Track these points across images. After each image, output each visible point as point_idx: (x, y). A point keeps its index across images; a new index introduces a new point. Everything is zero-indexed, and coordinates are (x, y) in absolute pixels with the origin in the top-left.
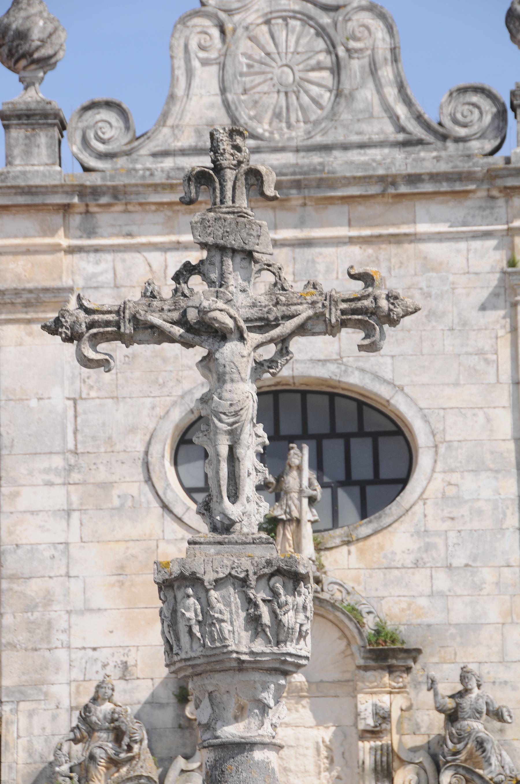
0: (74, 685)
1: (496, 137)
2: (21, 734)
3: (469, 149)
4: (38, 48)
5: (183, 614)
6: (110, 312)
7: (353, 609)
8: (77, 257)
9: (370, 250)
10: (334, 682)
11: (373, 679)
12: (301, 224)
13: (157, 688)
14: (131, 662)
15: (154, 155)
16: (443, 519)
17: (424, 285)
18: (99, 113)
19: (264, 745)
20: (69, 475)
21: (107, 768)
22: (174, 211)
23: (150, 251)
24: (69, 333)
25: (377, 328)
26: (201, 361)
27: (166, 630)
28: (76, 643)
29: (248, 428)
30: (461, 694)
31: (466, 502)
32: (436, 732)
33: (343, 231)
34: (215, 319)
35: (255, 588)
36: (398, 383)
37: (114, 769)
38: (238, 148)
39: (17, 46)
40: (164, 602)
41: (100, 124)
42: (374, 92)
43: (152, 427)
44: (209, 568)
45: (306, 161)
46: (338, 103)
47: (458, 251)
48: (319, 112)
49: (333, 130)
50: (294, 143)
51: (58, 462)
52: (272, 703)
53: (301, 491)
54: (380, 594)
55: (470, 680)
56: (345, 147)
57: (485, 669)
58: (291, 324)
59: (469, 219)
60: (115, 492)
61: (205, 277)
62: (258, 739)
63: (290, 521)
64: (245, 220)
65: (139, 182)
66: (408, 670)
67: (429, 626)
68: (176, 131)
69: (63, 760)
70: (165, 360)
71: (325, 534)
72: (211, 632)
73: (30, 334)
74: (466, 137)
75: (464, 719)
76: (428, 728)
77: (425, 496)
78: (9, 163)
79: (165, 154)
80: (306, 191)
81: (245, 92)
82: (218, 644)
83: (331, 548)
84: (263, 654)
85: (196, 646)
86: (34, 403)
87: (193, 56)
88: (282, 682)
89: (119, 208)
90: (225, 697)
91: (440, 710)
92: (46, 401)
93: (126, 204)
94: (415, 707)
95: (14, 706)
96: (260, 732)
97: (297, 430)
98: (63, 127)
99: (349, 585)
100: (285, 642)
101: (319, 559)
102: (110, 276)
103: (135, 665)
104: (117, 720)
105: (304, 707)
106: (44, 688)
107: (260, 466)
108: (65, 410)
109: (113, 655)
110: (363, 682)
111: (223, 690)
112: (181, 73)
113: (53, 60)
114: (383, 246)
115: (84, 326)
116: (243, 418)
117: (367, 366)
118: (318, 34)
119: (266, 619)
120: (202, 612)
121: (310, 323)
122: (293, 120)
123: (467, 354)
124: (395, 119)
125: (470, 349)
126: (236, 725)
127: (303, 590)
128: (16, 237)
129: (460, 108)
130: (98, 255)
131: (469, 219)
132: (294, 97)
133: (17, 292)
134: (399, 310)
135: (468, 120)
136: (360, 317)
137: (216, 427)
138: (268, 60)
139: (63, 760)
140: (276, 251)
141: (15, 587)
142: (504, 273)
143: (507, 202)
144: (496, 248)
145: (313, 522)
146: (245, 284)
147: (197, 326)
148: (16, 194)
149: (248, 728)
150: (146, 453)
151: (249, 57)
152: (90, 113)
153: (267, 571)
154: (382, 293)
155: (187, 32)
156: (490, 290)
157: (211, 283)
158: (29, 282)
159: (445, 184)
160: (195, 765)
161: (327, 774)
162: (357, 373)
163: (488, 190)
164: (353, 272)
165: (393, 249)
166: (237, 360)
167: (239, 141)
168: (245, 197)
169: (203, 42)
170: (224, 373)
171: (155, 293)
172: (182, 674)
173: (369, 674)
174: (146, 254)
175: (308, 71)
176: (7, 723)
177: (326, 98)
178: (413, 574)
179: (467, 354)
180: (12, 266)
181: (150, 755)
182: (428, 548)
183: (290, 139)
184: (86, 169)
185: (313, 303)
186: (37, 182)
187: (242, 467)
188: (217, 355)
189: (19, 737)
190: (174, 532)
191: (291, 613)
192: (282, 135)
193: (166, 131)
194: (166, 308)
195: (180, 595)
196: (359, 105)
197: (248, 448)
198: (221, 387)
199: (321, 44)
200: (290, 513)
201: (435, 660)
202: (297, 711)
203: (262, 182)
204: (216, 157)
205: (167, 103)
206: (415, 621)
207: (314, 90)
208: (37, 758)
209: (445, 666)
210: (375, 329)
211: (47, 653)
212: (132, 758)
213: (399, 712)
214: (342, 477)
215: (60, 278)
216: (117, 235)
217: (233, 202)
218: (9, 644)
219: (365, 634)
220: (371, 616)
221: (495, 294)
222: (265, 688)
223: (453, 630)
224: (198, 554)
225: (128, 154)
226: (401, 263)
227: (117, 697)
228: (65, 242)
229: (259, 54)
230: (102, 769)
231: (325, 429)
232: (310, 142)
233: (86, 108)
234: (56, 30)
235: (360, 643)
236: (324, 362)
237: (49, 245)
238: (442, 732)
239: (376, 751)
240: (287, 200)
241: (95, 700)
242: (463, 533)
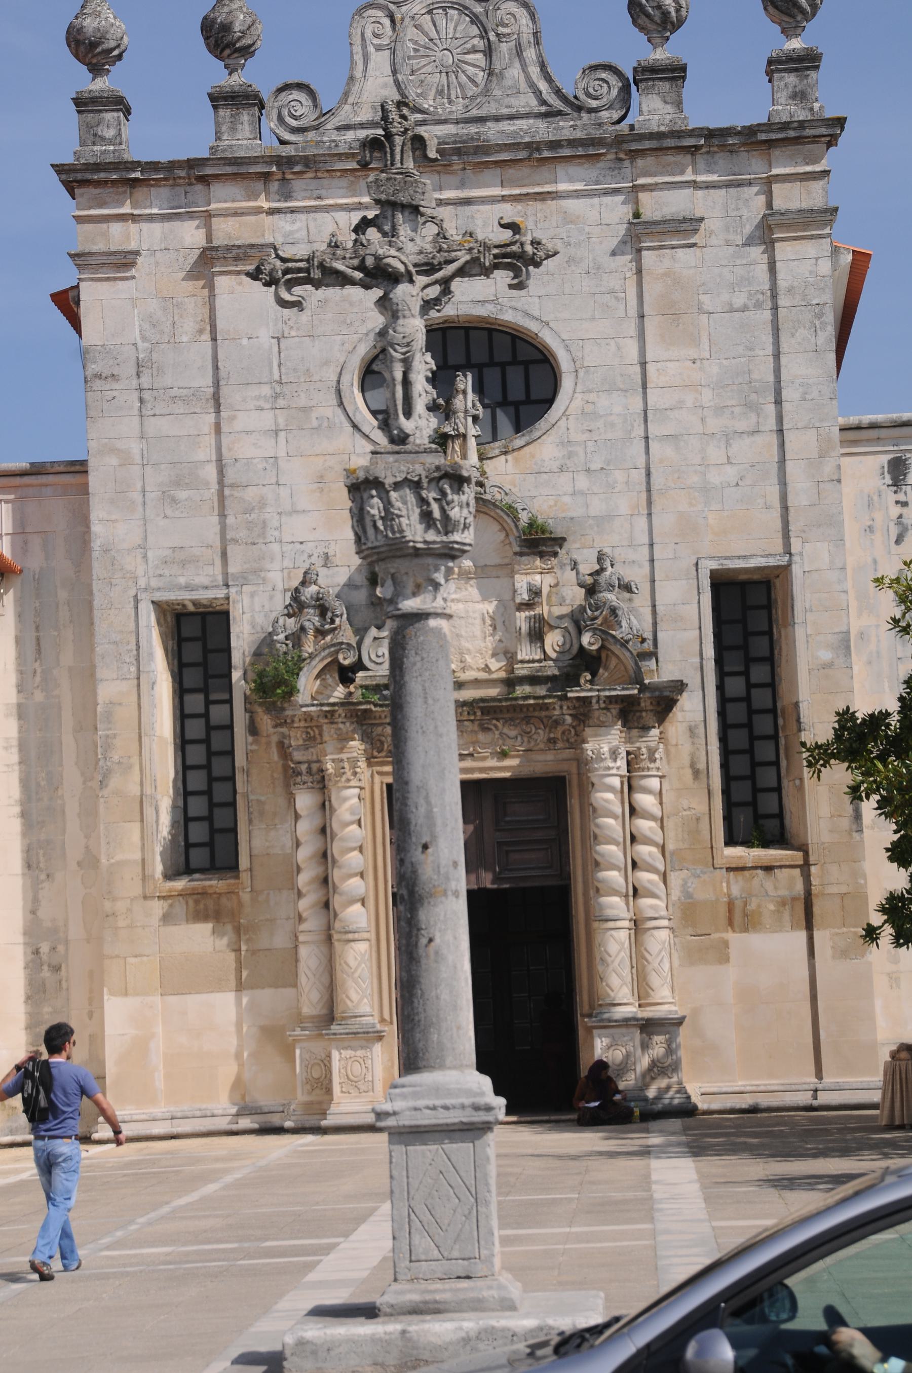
0: (286, 571)
2: (246, 610)
4: (239, 39)
5: (369, 512)
6: (301, 261)
7: (511, 507)
8: (276, 217)
9: (519, 207)
10: (495, 566)
11: (526, 562)
12: (462, 185)
13: (353, 573)
15: (338, 129)
16: (583, 432)
17: (564, 235)
18: (291, 94)
19: (437, 615)
20: (275, 402)
21: (315, 637)
24: (268, 278)
25: (524, 269)
26: (378, 301)
27: (355, 524)
28: (287, 538)
29: (418, 357)
30: (598, 573)
31: (601, 416)
32: (578, 602)
33: (497, 191)
34: (388, 265)
35: (427, 489)
37: (320, 638)
38: (404, 117)
39: (222, 37)
40: (353, 502)
41: (292, 103)
42: (521, 71)
43: (342, 360)
44: (389, 474)
47: (592, 206)
50: (454, 116)
51: (266, 390)
52: (442, 581)
53: (466, 411)
55: (605, 561)
56: (497, 119)
57: (618, 551)
58: (452, 268)
60: (314, 415)
61: (380, 230)
62: (432, 610)
63: (458, 436)
64: (411, 179)
66: (555, 554)
67: (572, 519)
68: (356, 108)
69: (280, 631)
70: (351, 304)
72: (392, 526)
73: (240, 284)
75: (601, 592)
76: (572, 600)
77: (567, 413)
78: (218, 138)
79: (347, 127)
81: (413, 73)
82: (398, 535)
83: (492, 458)
84: (434, 542)
85: (379, 537)
86: (245, 341)
87: (368, 42)
88: (451, 564)
90: (405, 578)
93: (316, 171)
94: (561, 584)
95: (239, 588)
96: (434, 604)
97: (462, 360)
98: (262, 106)
99: (507, 488)
100: (452, 532)
102: (305, 233)
103: (335, 556)
105: (472, 586)
106: (262, 574)
107: (429, 388)
108: (271, 348)
109: (316, 547)
110: (519, 565)
111: (403, 572)
112: (358, 57)
113: (252, 49)
115: (280, 273)
117: (519, 305)
118: (472, 22)
119: (437, 514)
121: (468, 266)
122: (453, 96)
123: (601, 293)
124: (538, 93)
125: (603, 289)
126: (414, 599)
128: (225, 201)
129: (592, 84)
130: (294, 215)
133: (228, 248)
134: (541, 254)
136: (509, 260)
137: (392, 356)
138: (431, 45)
139: (280, 631)
140: (441, 209)
141: (236, 494)
142: (630, 223)
143: (632, 163)
144: (623, 203)
145: (476, 437)
146: (413, 234)
147: (374, 271)
148: (224, 165)
149: (424, 602)
150: (338, 382)
151: (416, 43)
153: (436, 474)
155: (363, 22)
156: (619, 238)
157: (385, 234)
159: (580, 149)
160: (385, 633)
161: (491, 638)
162: (510, 311)
165: (539, 205)
166: (408, 299)
167: (405, 111)
168: (411, 159)
169: (376, 30)
170: (397, 311)
171: (339, 244)
173: (524, 558)
175: (465, 54)
176: (234, 602)
177: (481, 76)
178: (559, 476)
179: (601, 293)
181: (349, 626)
182: (570, 455)
184: (282, 142)
185: (471, 249)
186: (242, 154)
187: (414, 389)
188: (391, 296)
189: (243, 613)
191: (457, 509)
193: (347, 107)
194: (348, 256)
195: (365, 496)
196: (508, 82)
197: (419, 373)
198: (395, 323)
199: (475, 30)
200: (457, 430)
201: (577, 546)
202: (466, 589)
203: (425, 146)
205: (348, 84)
207: (471, 70)
208: (259, 629)
209: (585, 551)
210: (522, 270)
211: (264, 546)
212: (335, 629)
213: (549, 588)
214: (499, 398)
215: (263, 235)
216: (309, 198)
217: (402, 164)
218: (233, 539)
219: (520, 527)
221: (623, 242)
222: (437, 570)
223: (591, 522)
224: (380, 462)
225: (316, 128)
227: (321, 581)
228: (266, 205)
229: (423, 40)
231: (485, 359)
233: (280, 90)
234: (254, 22)
235: (517, 534)
237: (253, 208)
238: (583, 603)
239: (530, 618)
241: (303, 583)
242: (599, 442)
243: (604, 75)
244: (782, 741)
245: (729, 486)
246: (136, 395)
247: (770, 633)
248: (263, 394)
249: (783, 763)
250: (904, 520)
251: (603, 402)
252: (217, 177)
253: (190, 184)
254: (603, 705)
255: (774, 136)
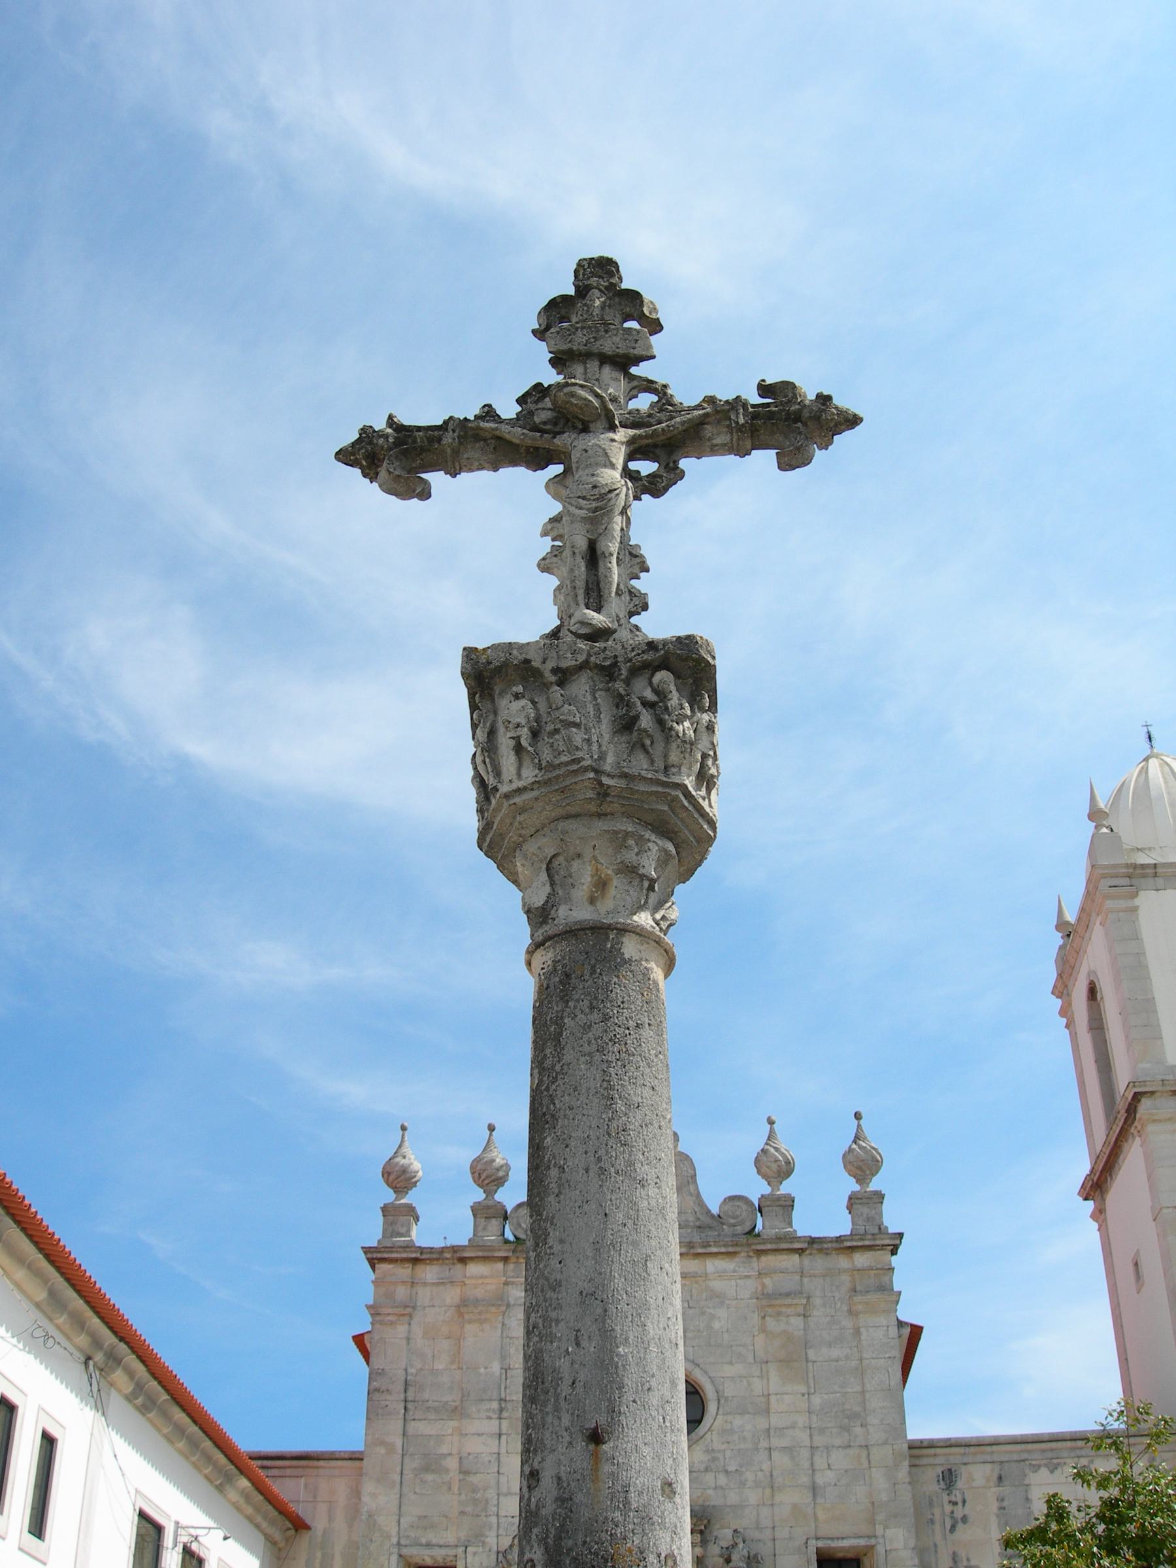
86: (482, 1370)
182: (714, 1459)
243: (738, 1203)
245: (830, 1485)
246: (402, 1405)
248: (492, 1407)
250: (955, 1515)
251: (738, 1421)
252: (472, 1259)
253: (453, 1264)
255: (855, 1244)
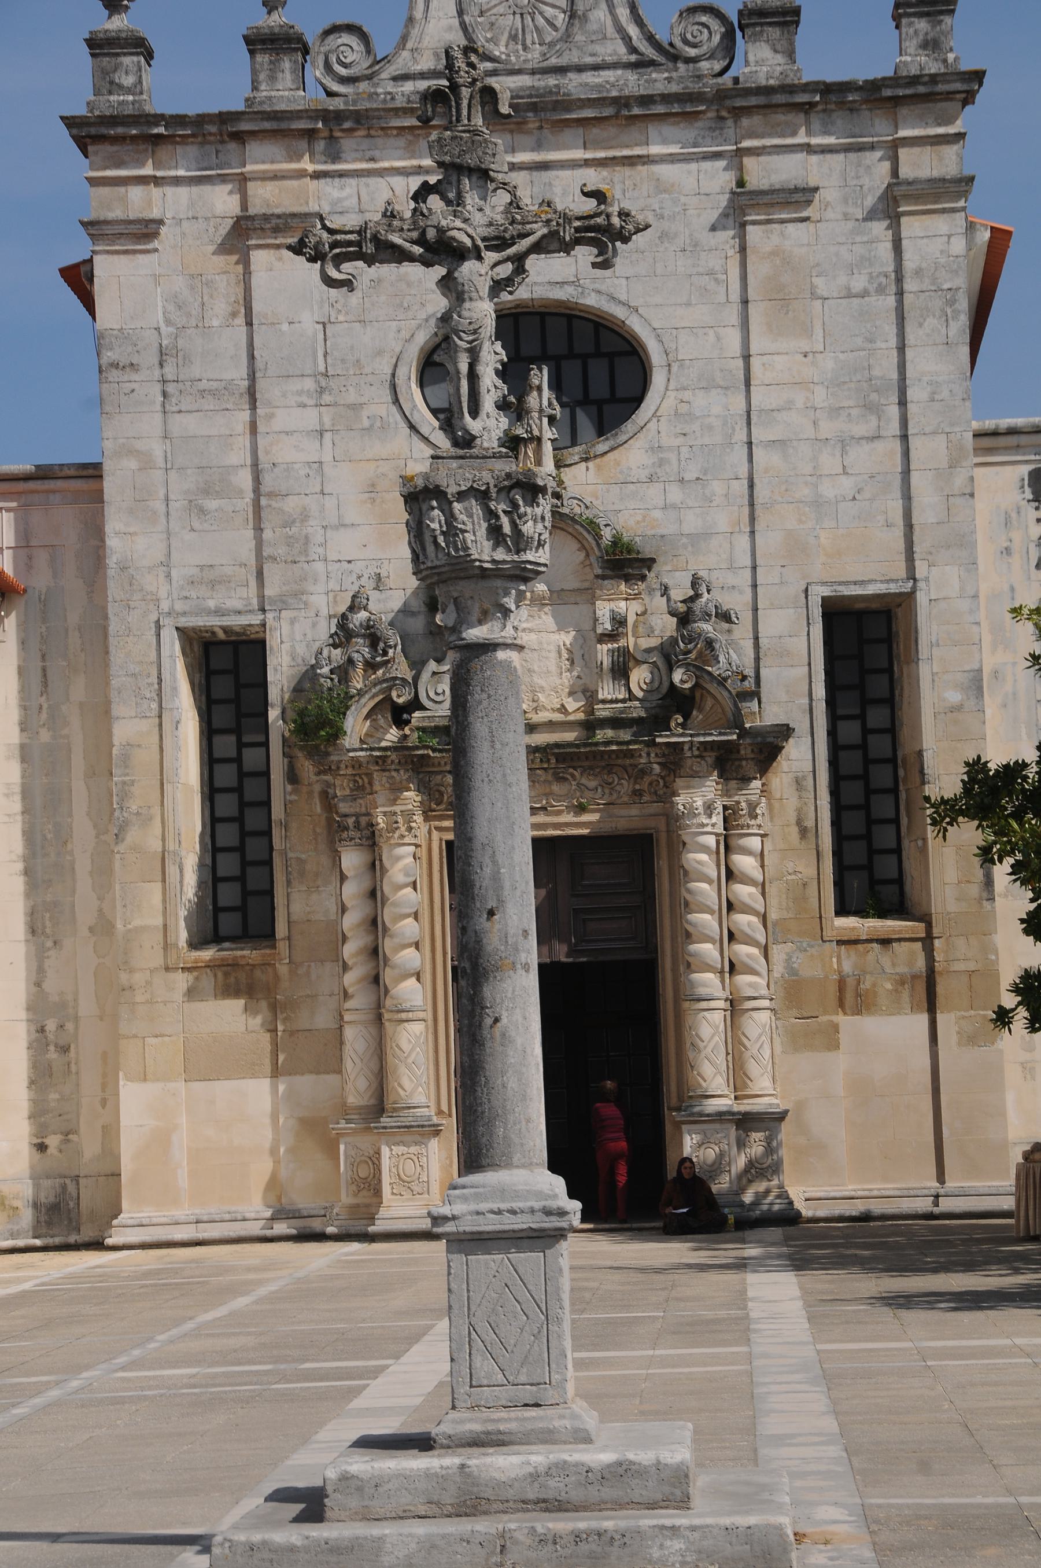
0: (331, 595)
1: (724, 58)
3: (699, 69)
7: (592, 522)
8: (322, 181)
9: (605, 173)
10: (573, 590)
11: (610, 587)
12: (538, 147)
14: (384, 574)
15: (395, 79)
16: (676, 436)
17: (656, 207)
18: (340, 37)
19: (506, 646)
20: (320, 397)
22: (415, 136)
23: (394, 175)
24: (312, 253)
26: (440, 281)
27: (413, 540)
28: (332, 556)
29: (486, 346)
31: (697, 418)
32: (669, 634)
33: (579, 154)
34: (453, 238)
36: (632, 304)
37: (370, 671)
38: (472, 65)
41: (342, 48)
42: (607, 13)
43: (398, 350)
45: (542, 83)
46: (573, 25)
47: (689, 172)
48: (554, 33)
49: (568, 52)
50: (529, 66)
52: (513, 607)
53: (541, 411)
54: (616, 507)
55: (700, 585)
56: (580, 69)
57: (715, 574)
59: (700, 140)
60: (365, 413)
61: (444, 198)
62: (501, 640)
65: (380, 106)
66: (643, 578)
67: (662, 536)
71: (565, 451)
72: (455, 542)
73: (280, 259)
74: (697, 57)
75: (695, 622)
76: (662, 631)
78: (255, 88)
79: (405, 77)
80: (543, 114)
81: (482, 14)
82: (462, 553)
84: (504, 562)
85: (440, 555)
86: (285, 327)
88: (523, 588)
89: (362, 133)
90: (469, 602)
91: (672, 613)
92: (297, 325)
93: (369, 129)
94: (649, 612)
96: (503, 634)
98: (306, 51)
100: (525, 550)
101: (558, 475)
103: (388, 577)
104: (372, 627)
106: (304, 598)
107: (499, 383)
114: (618, 168)
115: (327, 246)
116: (482, 336)
119: (507, 529)
120: (446, 523)
121: (545, 241)
122: (529, 42)
124: (627, 39)
125: (701, 270)
127: (541, 501)
128: (263, 162)
129: (690, 28)
130: (343, 180)
131: (700, 140)
132: (530, 19)
135: (698, 40)
137: (456, 345)
141: (274, 504)
142: (733, 193)
143: (736, 122)
144: (725, 169)
145: (552, 441)
146: (482, 203)
147: (435, 246)
148: (262, 119)
149: (492, 631)
150: (393, 375)
152: (332, 37)
154: (614, 209)
156: (720, 210)
157: (448, 202)
158: (277, 208)
160: (446, 668)
162: (593, 294)
163: (718, 111)
164: (586, 190)
165: (627, 171)
166: (475, 278)
168: (480, 115)
171: (395, 213)
172: (429, 581)
174: (388, 179)
176: (271, 629)
177: (561, 19)
178: (648, 488)
180: (261, 191)
182: (661, 462)
183: (525, 61)
184: (330, 94)
185: (548, 222)
186: (282, 107)
188: (456, 275)
189: (282, 642)
190: (422, 451)
191: (530, 523)
192: (518, 57)
193: (405, 54)
195: (424, 507)
196: (592, 26)
198: (460, 306)
200: (531, 433)
201: (669, 568)
204: (451, 75)
205: (406, 26)
206: (650, 533)
207: (549, 11)
208: (300, 661)
209: (677, 574)
210: (607, 246)
214: (580, 396)
215: (307, 203)
216: (361, 160)
217: (469, 120)
218: (270, 557)
220: (609, 528)
221: (725, 215)
222: (507, 594)
223: (684, 540)
224: (441, 468)
226: (635, 185)
227: (371, 606)
228: (310, 168)
230: (360, 672)
232: (545, 64)
233: (327, 33)
236: (562, 284)
238: (675, 634)
239: (613, 652)
240: (525, 123)
241: (352, 608)
244: (903, 796)
246: (157, 388)
247: (890, 671)
249: (904, 821)
251: (700, 401)
252: (253, 133)
253: (222, 142)
254: (696, 753)
